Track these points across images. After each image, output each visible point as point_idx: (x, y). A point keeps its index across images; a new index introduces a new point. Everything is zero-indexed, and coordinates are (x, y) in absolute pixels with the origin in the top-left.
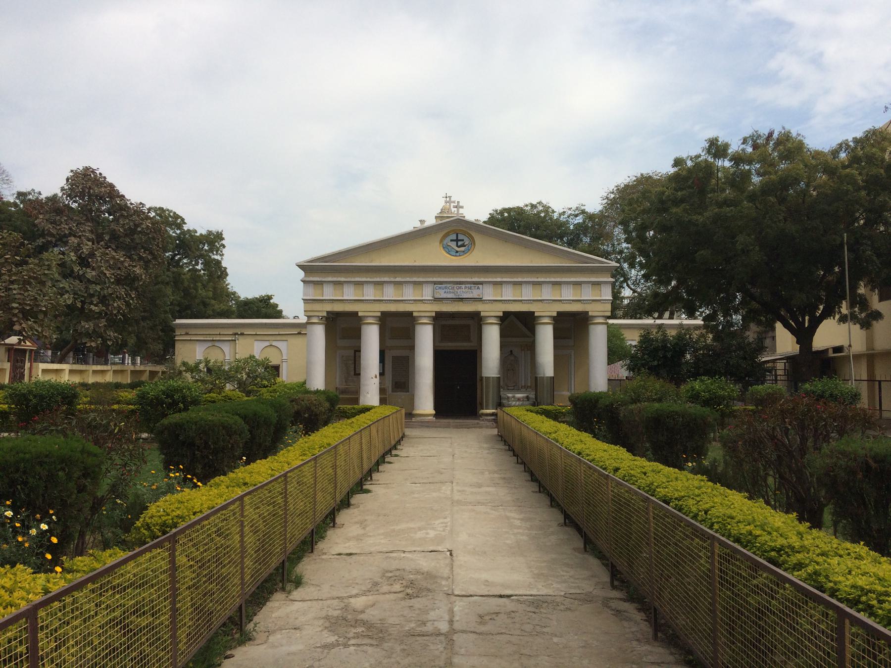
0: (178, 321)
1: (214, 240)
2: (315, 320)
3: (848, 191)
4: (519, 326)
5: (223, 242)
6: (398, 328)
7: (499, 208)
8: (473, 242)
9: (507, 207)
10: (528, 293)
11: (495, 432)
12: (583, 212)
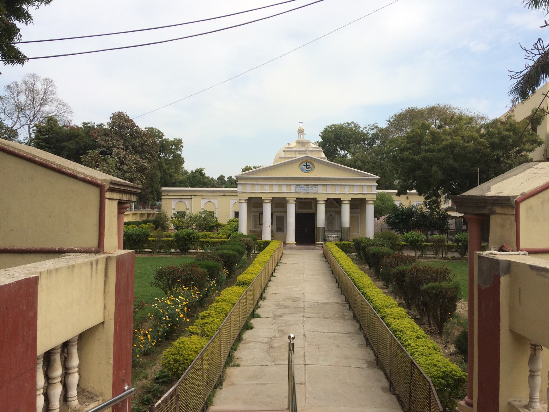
0: (163, 189)
1: (178, 144)
2: (243, 201)
3: (481, 149)
4: (334, 205)
5: (182, 144)
6: (279, 205)
7: (330, 125)
8: (314, 166)
9: (334, 124)
10: (338, 190)
11: (322, 252)
12: (377, 127)
